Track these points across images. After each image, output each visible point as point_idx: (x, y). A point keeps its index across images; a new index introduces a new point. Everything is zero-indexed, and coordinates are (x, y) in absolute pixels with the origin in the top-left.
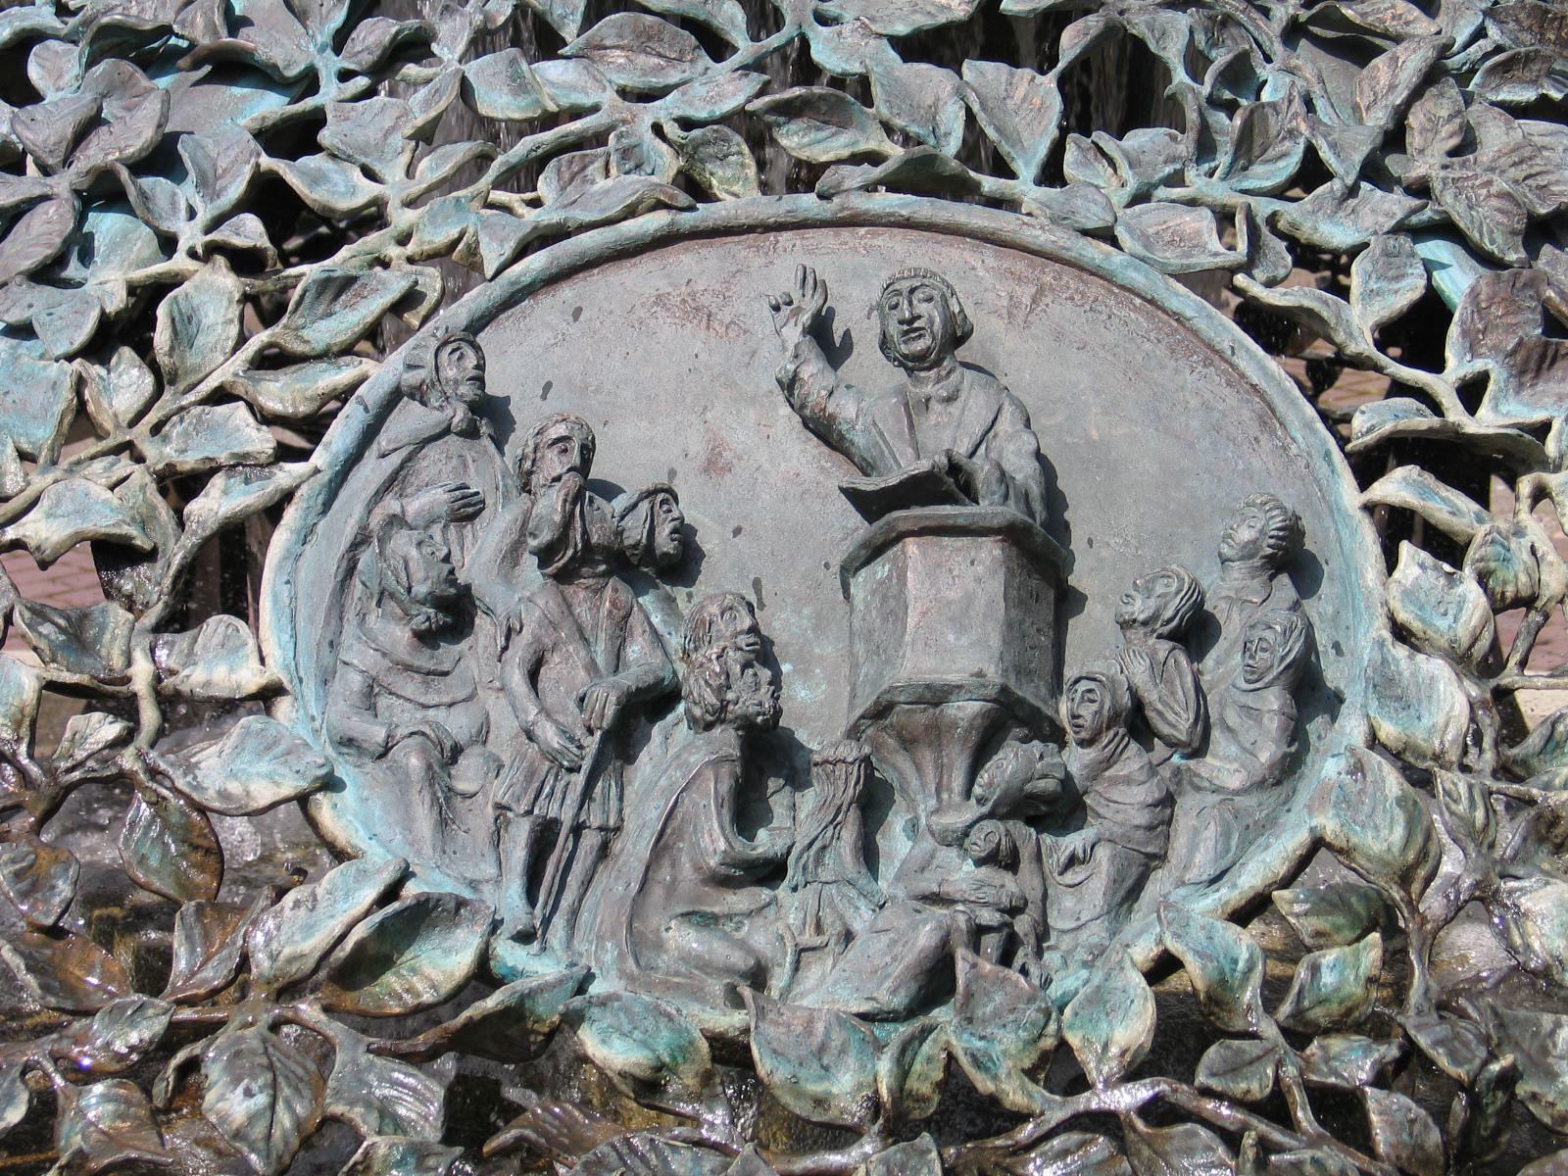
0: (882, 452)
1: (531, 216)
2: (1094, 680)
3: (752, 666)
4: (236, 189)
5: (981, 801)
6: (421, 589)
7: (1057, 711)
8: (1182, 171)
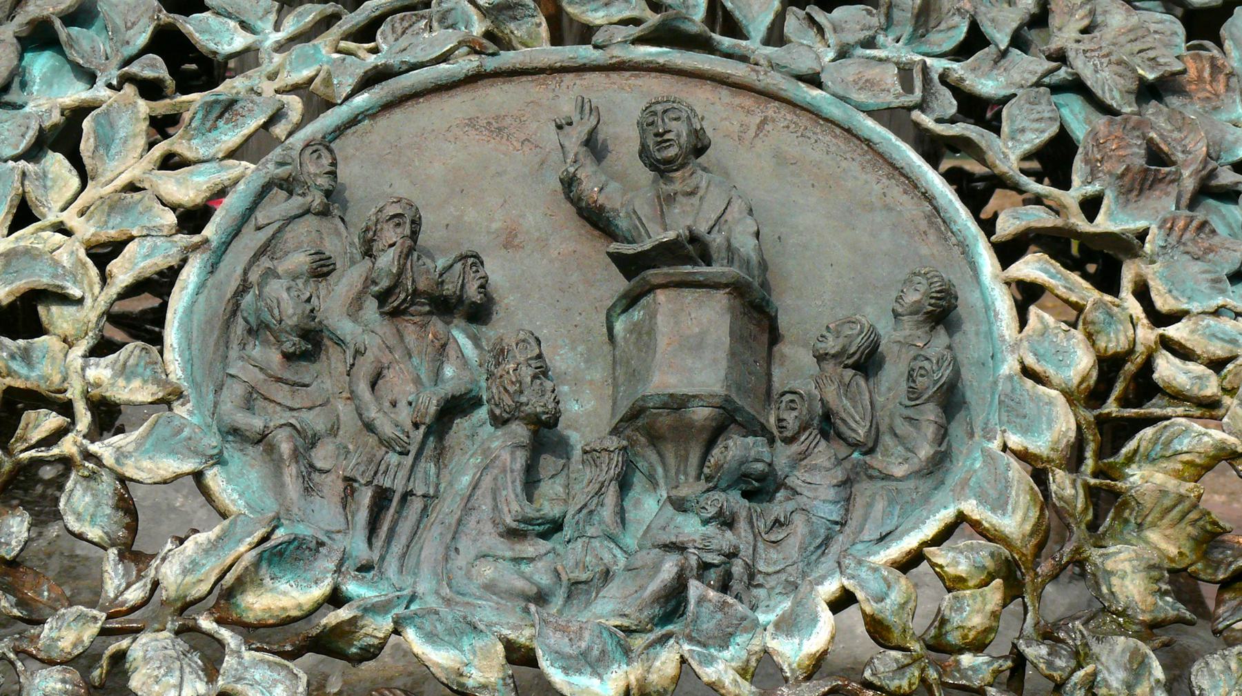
0: (640, 232)
1: (372, 60)
2: (795, 393)
3: (539, 378)
4: (142, 39)
5: (708, 479)
6: (292, 321)
7: (768, 421)
8: (874, 38)
